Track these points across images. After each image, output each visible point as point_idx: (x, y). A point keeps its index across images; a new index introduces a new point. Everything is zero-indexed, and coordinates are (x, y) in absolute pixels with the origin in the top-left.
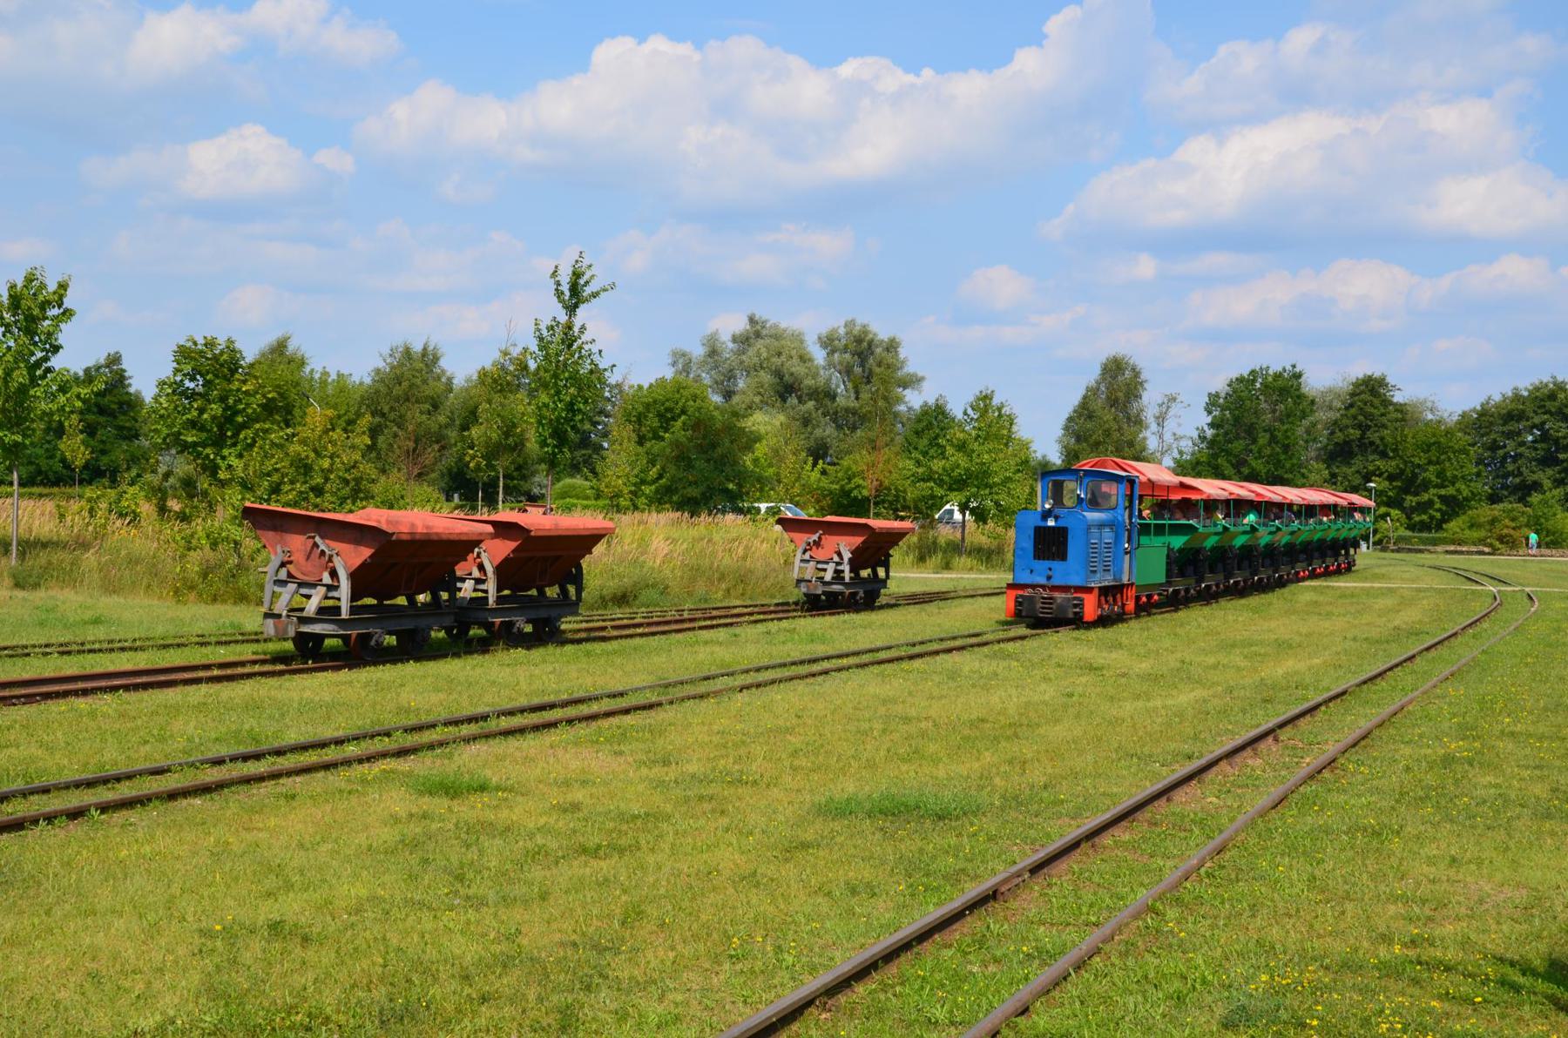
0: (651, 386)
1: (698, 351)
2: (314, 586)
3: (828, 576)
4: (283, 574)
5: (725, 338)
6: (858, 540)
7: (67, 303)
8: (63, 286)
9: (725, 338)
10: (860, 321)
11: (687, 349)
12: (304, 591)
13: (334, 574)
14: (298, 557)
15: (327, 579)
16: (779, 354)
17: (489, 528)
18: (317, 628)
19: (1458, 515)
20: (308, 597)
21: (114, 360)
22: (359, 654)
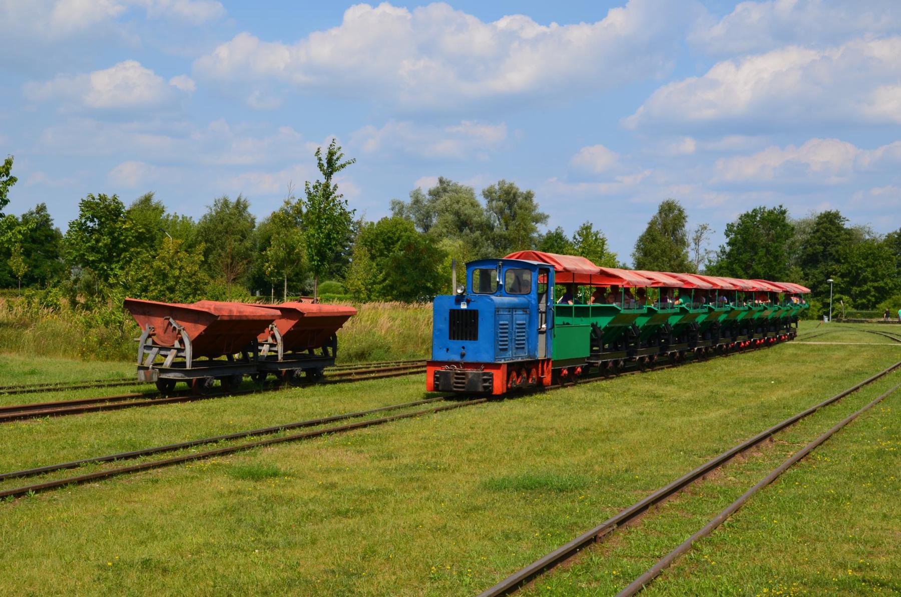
1: (408, 201)
2: (169, 349)
4: (150, 342)
5: (425, 192)
7: (12, 173)
9: (425, 192)
10: (508, 181)
13: (181, 342)
14: (159, 331)
15: (177, 344)
16: (458, 202)
18: (171, 376)
20: (166, 356)
22: (197, 391)
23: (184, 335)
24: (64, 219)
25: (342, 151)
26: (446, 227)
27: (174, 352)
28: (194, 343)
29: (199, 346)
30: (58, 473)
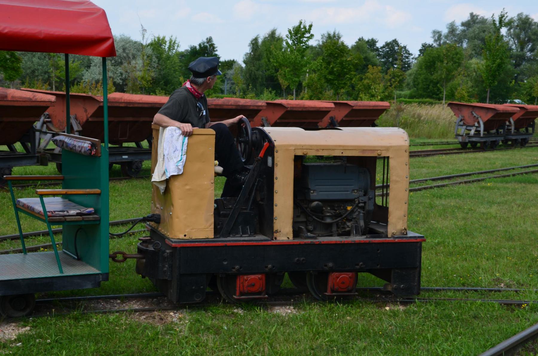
0: (425, 49)
1: (445, 31)
2: (472, 126)
3: (472, 132)
4: (462, 123)
5: (458, 23)
6: (489, 115)
7: (312, 32)
8: (311, 26)
9: (458, 23)
10: (525, 13)
11: (439, 29)
12: (469, 128)
13: (479, 123)
14: (467, 118)
15: (476, 124)
16: (484, 31)
17: (518, 109)
18: (474, 139)
19: (277, 79)
20: (470, 130)
21: (210, 40)
22: (485, 147)
23: (480, 119)
24: (233, 50)
25: (508, 14)
26: (474, 50)
27: (475, 128)
28: (485, 124)
29: (488, 125)
30: (496, 173)
